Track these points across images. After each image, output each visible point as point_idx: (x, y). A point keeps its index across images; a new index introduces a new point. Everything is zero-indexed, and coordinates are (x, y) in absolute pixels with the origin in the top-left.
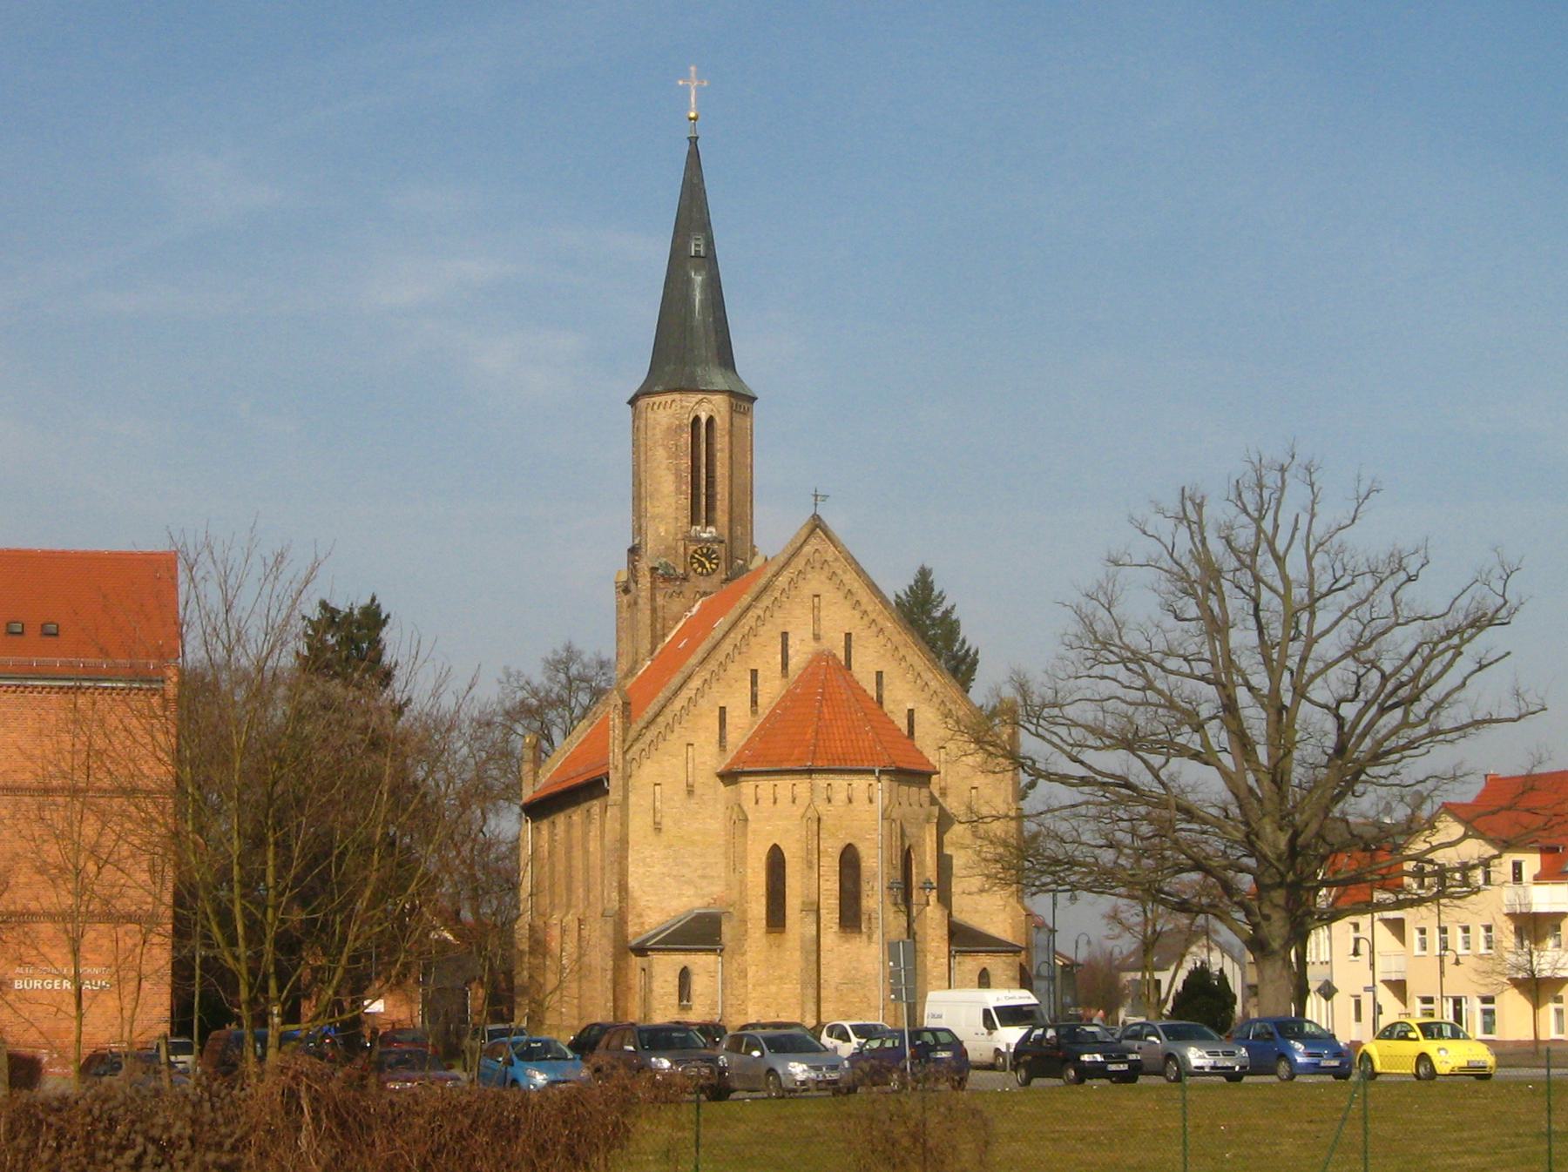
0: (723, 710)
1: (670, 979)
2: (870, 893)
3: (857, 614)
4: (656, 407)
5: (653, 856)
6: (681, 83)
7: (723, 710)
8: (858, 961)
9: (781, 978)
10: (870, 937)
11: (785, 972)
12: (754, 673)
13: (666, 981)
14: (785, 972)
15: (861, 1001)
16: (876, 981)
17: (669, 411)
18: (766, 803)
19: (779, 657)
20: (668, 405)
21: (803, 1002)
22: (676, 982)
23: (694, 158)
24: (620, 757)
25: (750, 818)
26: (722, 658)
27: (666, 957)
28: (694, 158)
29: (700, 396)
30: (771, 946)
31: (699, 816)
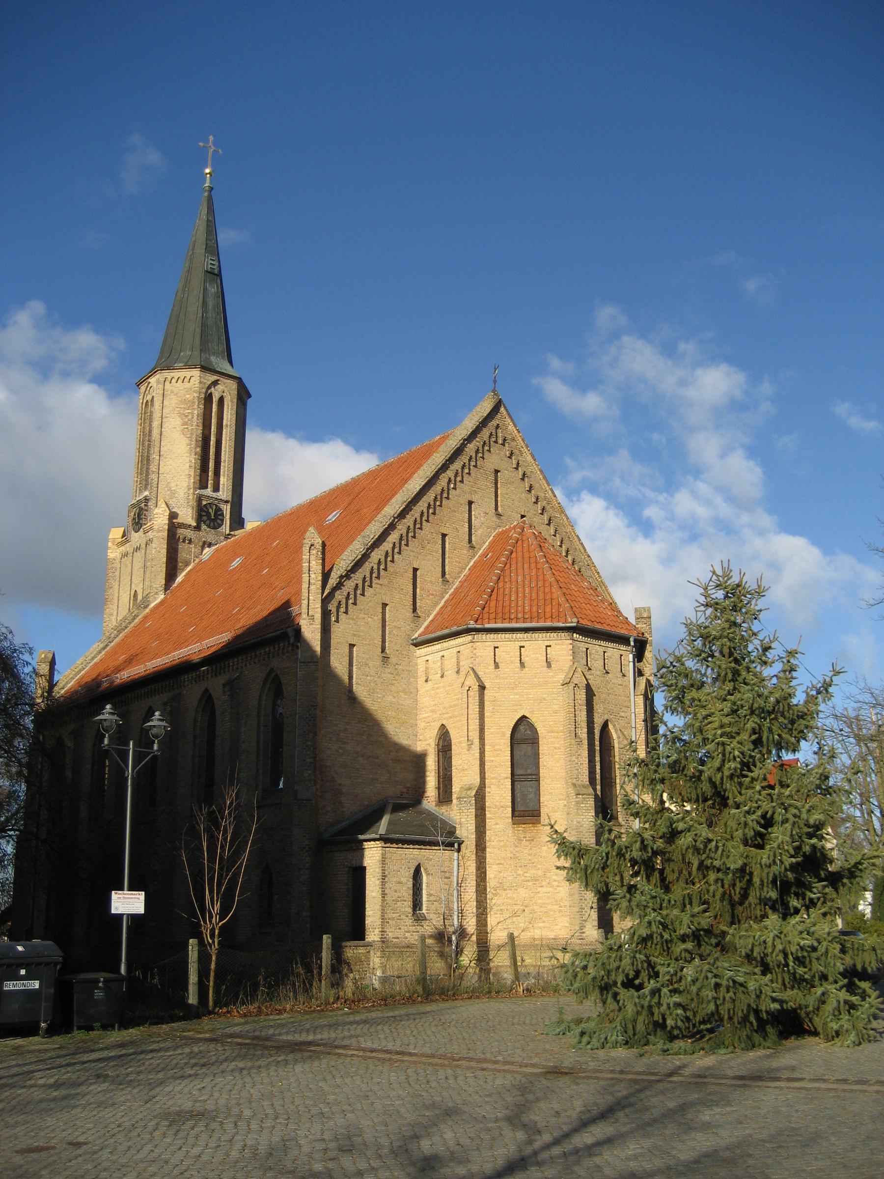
1: (404, 880)
4: (174, 381)
5: (346, 729)
6: (201, 144)
9: (535, 879)
11: (540, 873)
13: (400, 883)
14: (540, 873)
17: (187, 385)
18: (510, 664)
24: (319, 605)
26: (417, 515)
27: (400, 851)
29: (215, 378)
31: (393, 688)
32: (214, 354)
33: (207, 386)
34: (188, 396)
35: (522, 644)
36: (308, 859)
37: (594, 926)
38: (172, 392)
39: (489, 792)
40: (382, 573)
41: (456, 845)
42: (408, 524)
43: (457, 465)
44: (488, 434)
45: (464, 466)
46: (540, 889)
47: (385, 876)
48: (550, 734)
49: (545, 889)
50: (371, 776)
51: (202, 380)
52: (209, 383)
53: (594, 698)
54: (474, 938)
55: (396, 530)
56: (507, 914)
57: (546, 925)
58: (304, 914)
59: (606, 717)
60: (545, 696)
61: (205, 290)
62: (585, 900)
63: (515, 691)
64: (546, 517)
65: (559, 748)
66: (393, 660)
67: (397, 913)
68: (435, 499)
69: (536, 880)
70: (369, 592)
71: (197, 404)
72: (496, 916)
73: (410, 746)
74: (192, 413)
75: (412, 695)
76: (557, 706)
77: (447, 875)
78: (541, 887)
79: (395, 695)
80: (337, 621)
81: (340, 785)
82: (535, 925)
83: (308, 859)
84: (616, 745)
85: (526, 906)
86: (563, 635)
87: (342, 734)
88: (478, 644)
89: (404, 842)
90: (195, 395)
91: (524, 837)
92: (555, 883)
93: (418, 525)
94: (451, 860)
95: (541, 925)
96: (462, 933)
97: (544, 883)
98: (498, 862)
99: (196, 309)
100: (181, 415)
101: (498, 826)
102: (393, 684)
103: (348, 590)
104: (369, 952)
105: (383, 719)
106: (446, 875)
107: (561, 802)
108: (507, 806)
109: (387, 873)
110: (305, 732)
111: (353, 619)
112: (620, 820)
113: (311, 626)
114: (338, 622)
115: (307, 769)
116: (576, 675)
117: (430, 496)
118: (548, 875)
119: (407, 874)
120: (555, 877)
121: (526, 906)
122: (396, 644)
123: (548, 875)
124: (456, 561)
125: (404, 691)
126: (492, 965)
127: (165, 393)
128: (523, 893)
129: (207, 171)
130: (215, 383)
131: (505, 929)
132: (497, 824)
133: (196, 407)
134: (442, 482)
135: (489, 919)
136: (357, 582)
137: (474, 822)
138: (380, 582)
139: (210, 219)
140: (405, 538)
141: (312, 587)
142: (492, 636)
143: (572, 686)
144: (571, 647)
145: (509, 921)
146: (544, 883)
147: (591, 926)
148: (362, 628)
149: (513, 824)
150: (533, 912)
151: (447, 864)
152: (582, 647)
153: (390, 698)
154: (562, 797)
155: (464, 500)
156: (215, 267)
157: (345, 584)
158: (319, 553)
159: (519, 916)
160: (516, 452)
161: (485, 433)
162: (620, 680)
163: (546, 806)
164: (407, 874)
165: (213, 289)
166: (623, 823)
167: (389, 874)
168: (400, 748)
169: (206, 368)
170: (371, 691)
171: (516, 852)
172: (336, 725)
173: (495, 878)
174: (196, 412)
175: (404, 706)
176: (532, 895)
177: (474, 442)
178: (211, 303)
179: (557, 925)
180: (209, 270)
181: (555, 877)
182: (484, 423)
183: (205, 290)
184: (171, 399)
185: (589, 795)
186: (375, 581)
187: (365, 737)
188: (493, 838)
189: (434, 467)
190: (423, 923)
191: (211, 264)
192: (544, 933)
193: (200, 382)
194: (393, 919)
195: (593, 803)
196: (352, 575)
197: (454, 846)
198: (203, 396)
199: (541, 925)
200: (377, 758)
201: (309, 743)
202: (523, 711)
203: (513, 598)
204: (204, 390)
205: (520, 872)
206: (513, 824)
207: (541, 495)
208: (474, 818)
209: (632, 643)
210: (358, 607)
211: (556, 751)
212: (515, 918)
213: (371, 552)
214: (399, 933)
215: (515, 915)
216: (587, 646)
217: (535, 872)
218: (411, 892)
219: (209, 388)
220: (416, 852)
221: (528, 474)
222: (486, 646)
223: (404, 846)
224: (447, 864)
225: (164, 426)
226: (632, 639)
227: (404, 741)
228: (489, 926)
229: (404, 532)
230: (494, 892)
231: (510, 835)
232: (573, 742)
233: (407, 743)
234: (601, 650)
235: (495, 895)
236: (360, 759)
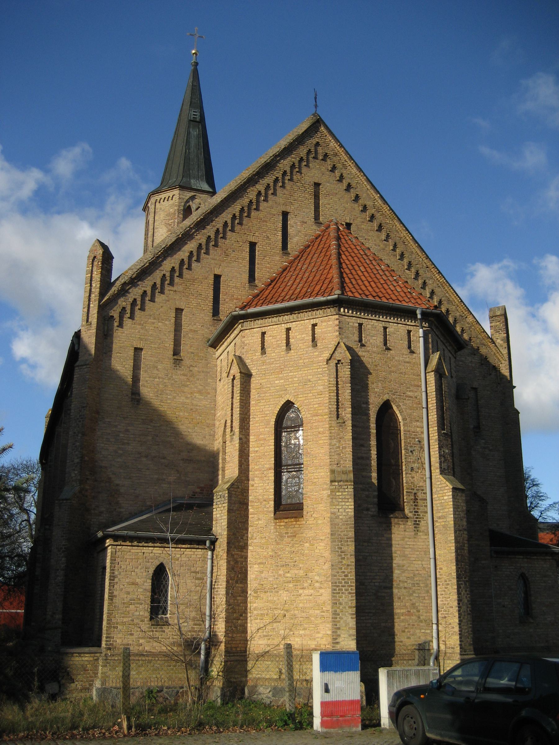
0: (217, 278)
2: (415, 465)
3: (358, 208)
4: (162, 201)
5: (127, 431)
7: (217, 278)
8: (195, 668)
9: (296, 580)
10: (416, 524)
11: (301, 573)
12: (253, 245)
14: (301, 573)
15: (409, 613)
16: (427, 586)
19: (280, 234)
20: (170, 198)
21: (335, 613)
22: (148, 585)
23: (195, 74)
25: (253, 372)
26: (220, 226)
27: (135, 550)
28: (195, 74)
29: (193, 194)
30: (281, 536)
31: (186, 389)
32: (194, 178)
33: (185, 200)
34: (171, 210)
35: (288, 326)
36: (63, 559)
37: (350, 636)
38: (161, 209)
39: (253, 486)
40: (177, 280)
41: (208, 543)
42: (209, 234)
43: (269, 179)
44: (305, 151)
45: (276, 180)
46: (301, 591)
47: (114, 577)
48: (314, 418)
49: (306, 592)
50: (156, 476)
51: (181, 196)
52: (187, 198)
53: (369, 376)
54: (222, 647)
55: (193, 240)
56: (267, 620)
57: (307, 632)
58: (57, 616)
59: (386, 397)
60: (309, 377)
61: (189, 133)
62: (340, 604)
63: (280, 376)
64: (375, 225)
65: (323, 433)
66: (187, 362)
67: (129, 617)
68: (242, 210)
69: (298, 581)
70: (159, 298)
71: (177, 215)
72: (257, 621)
73: (206, 446)
74: (174, 222)
75: (209, 396)
76: (322, 387)
77: (199, 576)
78: (302, 589)
79: (189, 396)
80: (121, 325)
81: (118, 485)
82: (296, 633)
83: (63, 559)
84: (402, 428)
85: (287, 611)
86: (329, 311)
87: (122, 435)
88: (246, 331)
89: (140, 539)
90: (176, 208)
91: (286, 533)
92: (317, 585)
93: (221, 234)
94: (204, 561)
95: (302, 632)
96: (212, 641)
97: (306, 585)
98: (259, 561)
99: (181, 148)
100: (167, 225)
101: (260, 522)
102: (187, 386)
103: (134, 297)
104: (97, 659)
105: (175, 420)
106: (199, 576)
107: (325, 492)
108: (269, 500)
109: (116, 573)
110: (74, 433)
111: (140, 324)
112: (407, 511)
113: (89, 331)
114: (122, 328)
115: (74, 470)
116: (339, 350)
117: (236, 208)
118: (310, 574)
119: (145, 574)
120: (317, 578)
121: (287, 611)
122: (191, 347)
123: (310, 574)
124: (266, 267)
125: (200, 392)
126: (250, 676)
127: (156, 211)
128: (284, 596)
129: (194, 52)
130: (193, 198)
131: (264, 636)
132: (259, 519)
133: (176, 217)
134: (251, 194)
135: (249, 625)
136: (145, 289)
137: (226, 517)
138: (175, 288)
139: (195, 84)
140: (204, 247)
141: (93, 296)
142: (259, 322)
143: (333, 363)
144: (337, 322)
145: (269, 627)
146: (306, 585)
147: (346, 636)
148: (150, 333)
149: (275, 519)
150: (294, 617)
151: (199, 564)
152: (354, 322)
153: (182, 399)
154: (325, 486)
155: (278, 210)
156: (197, 117)
157: (130, 291)
158: (100, 263)
159: (280, 622)
160: (339, 165)
161: (302, 151)
162: (408, 357)
163: (309, 497)
164: (145, 574)
165: (195, 133)
166: (410, 515)
167: (120, 574)
168: (192, 448)
169: (182, 188)
170: (159, 392)
171: (278, 549)
172: (116, 426)
173: (256, 579)
174: (176, 221)
175: (200, 406)
176: (293, 598)
177: (289, 158)
178: (193, 142)
179: (318, 633)
180: (192, 119)
181: (317, 578)
182: (300, 140)
183: (189, 133)
184: (160, 214)
185: (347, 481)
186: (167, 288)
187: (150, 438)
188: (255, 535)
189: (239, 182)
190: (165, 628)
191: (194, 114)
192: (304, 642)
193: (180, 198)
194: (123, 623)
195: (352, 490)
196: (139, 283)
197: (205, 545)
198: (182, 208)
199: (302, 632)
200: (164, 458)
201: (78, 444)
202: (288, 396)
203: (289, 284)
204: (183, 204)
205: (281, 572)
206: (275, 519)
207: (369, 203)
208: (226, 514)
209: (419, 316)
210: (147, 312)
211: (320, 436)
212: (275, 625)
213: (162, 261)
214: (130, 640)
215: (275, 620)
216: (359, 321)
217: (297, 572)
218: (149, 594)
219: (187, 201)
220: (157, 551)
221: (353, 184)
222: (254, 333)
223: (140, 544)
224: (199, 564)
225: (155, 235)
226: (418, 312)
227: (198, 440)
228: (249, 631)
229: (203, 241)
230: (255, 595)
231: (272, 531)
232: (334, 423)
233: (202, 442)
234: (380, 325)
235: (257, 597)
236: (144, 459)
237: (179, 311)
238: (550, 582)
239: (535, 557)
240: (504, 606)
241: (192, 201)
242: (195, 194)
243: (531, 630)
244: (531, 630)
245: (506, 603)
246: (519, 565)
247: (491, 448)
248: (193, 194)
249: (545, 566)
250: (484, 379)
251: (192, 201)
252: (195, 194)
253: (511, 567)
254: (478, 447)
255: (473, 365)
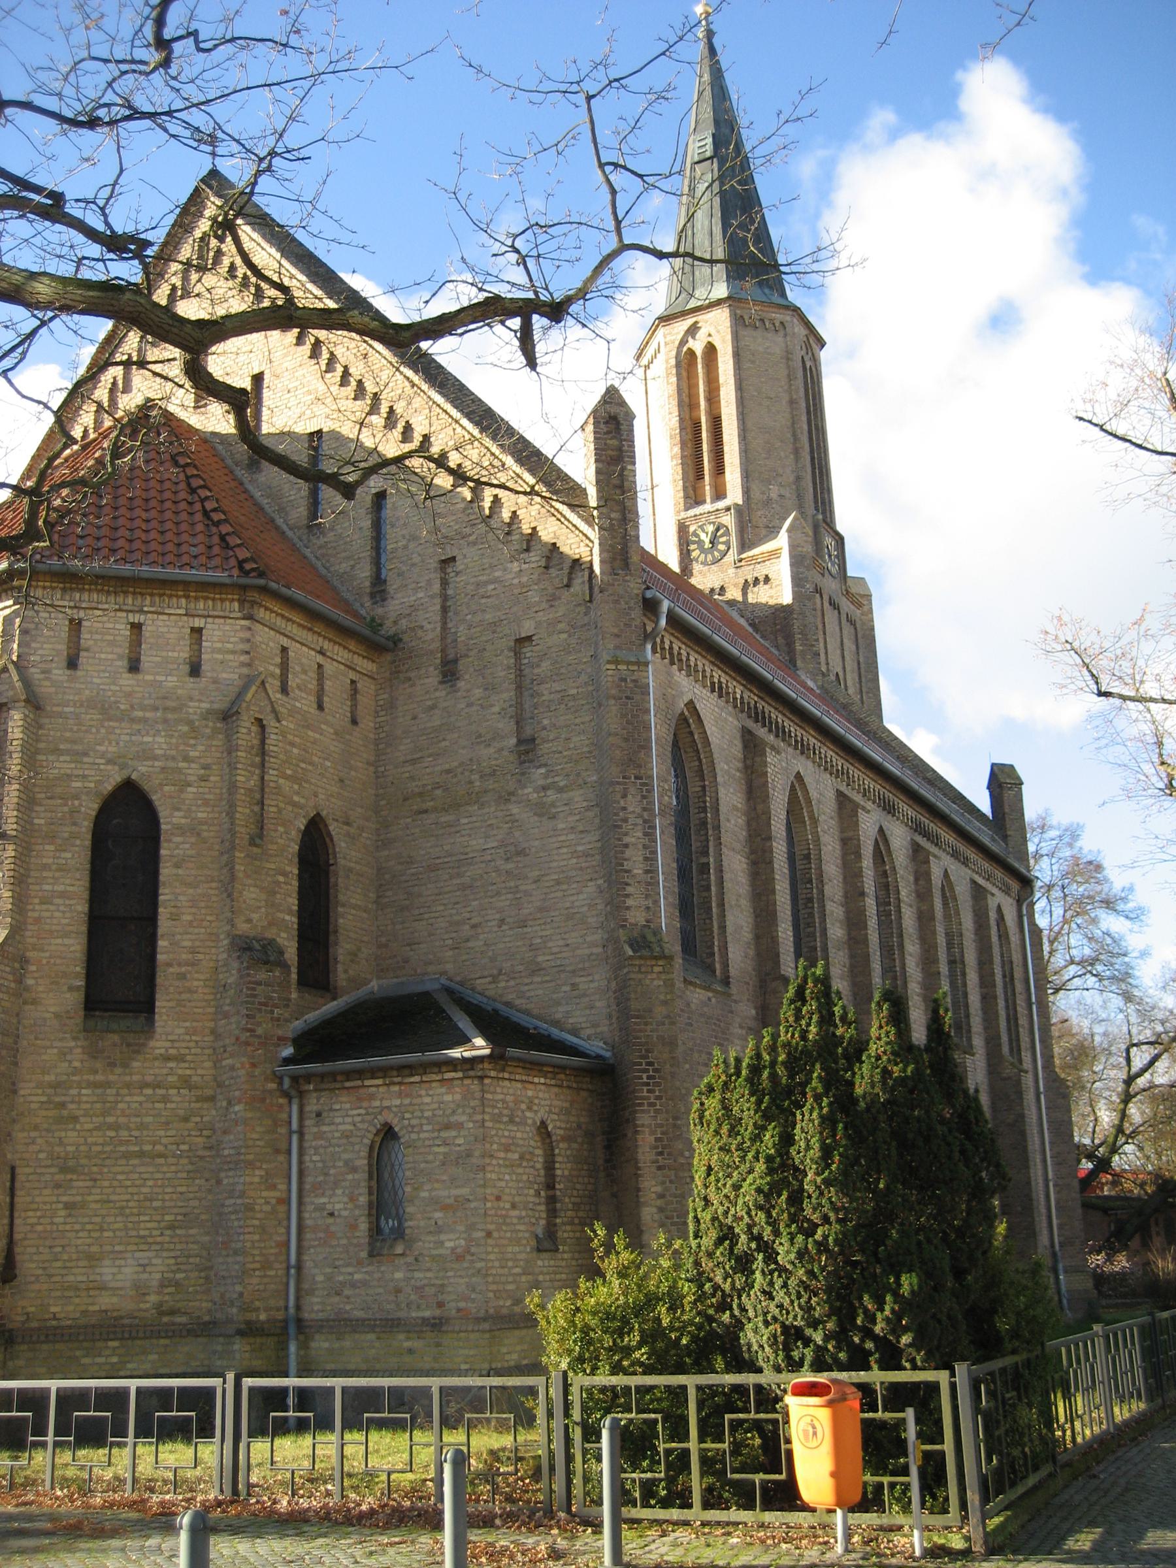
29: (689, 322)
33: (677, 343)
130: (693, 330)
219: (683, 342)
237: (134, 666)
238: (460, 1141)
239: (417, 1079)
240: (332, 1214)
241: (694, 338)
242: (694, 319)
243: (399, 1275)
244: (399, 1275)
245: (338, 1206)
246: (377, 1103)
247: (562, 784)
248: (689, 322)
249: (448, 1098)
250: (552, 606)
251: (694, 338)
252: (694, 319)
253: (355, 1112)
254: (526, 791)
255: (524, 579)
